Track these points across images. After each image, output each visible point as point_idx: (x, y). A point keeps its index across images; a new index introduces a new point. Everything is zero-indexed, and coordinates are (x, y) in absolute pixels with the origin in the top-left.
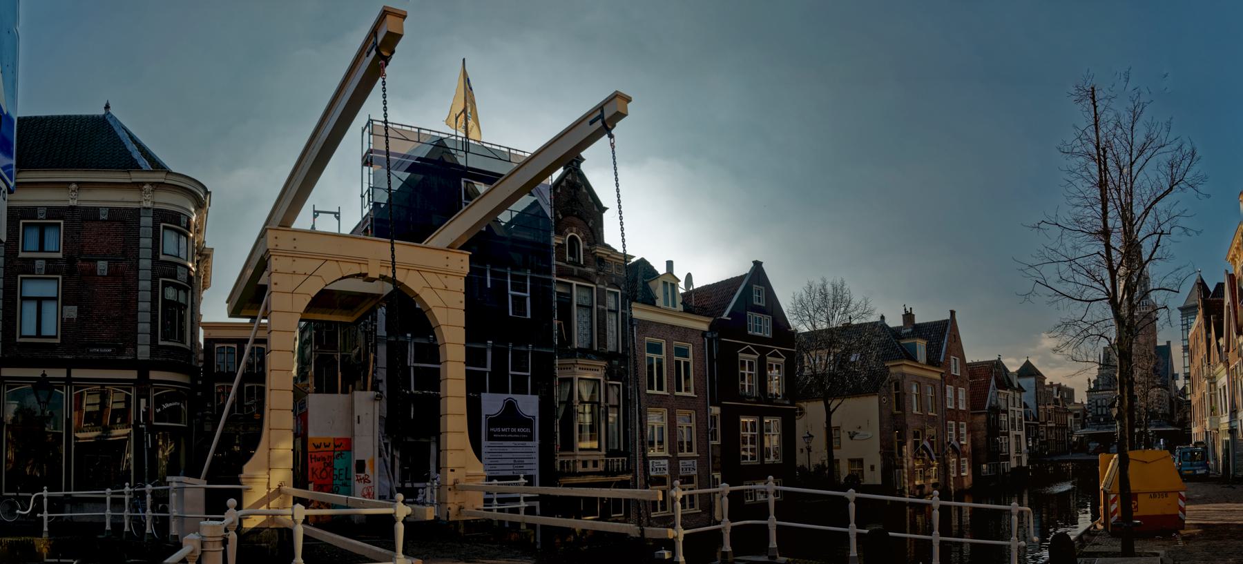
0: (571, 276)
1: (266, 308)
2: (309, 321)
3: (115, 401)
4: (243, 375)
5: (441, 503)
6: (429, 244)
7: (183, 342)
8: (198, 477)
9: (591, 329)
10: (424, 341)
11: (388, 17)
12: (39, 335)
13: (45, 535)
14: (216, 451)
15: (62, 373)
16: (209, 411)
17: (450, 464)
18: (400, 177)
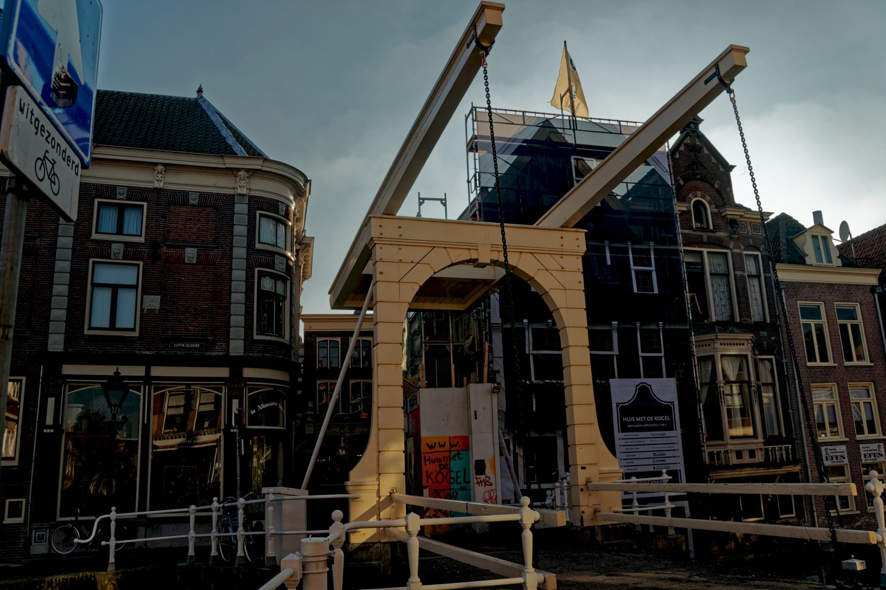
0: (701, 243)
1: (372, 299)
2: (417, 311)
3: (203, 403)
4: (348, 370)
5: (573, 506)
6: (541, 225)
7: (281, 336)
8: (299, 487)
10: (542, 326)
11: (486, 10)
12: (112, 326)
13: (111, 568)
14: (319, 456)
15: (139, 371)
16: (309, 413)
17: (580, 461)
18: (506, 161)
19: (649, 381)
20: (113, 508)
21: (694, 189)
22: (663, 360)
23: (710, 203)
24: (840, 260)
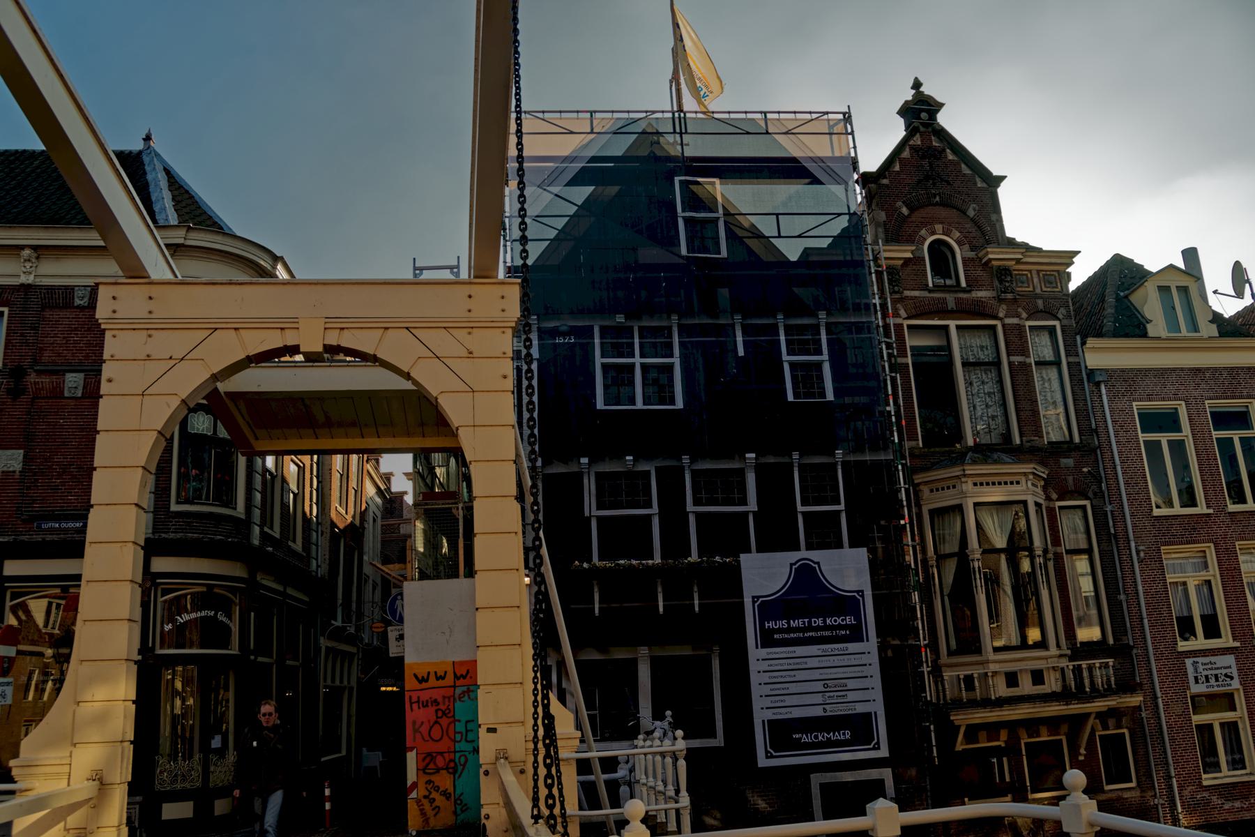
0: (945, 313)
9: (1004, 405)
19: (815, 555)
21: (929, 223)
22: (843, 516)
23: (959, 243)
24: (1214, 326)
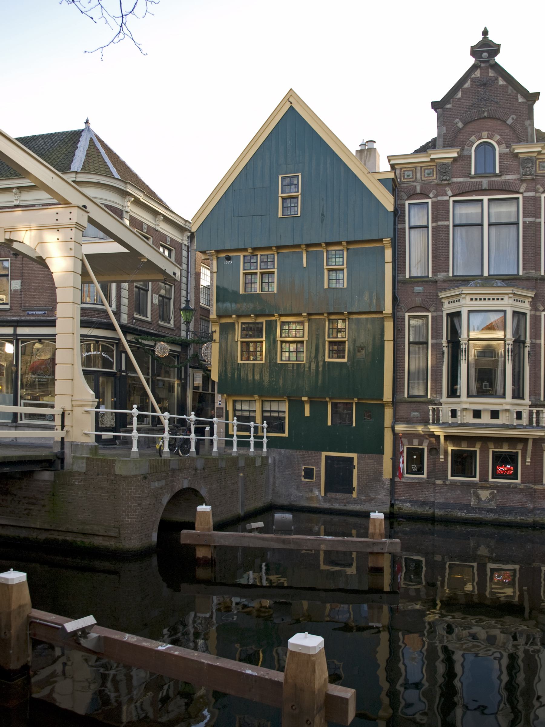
20: (135, 406)
23: (499, 143)
